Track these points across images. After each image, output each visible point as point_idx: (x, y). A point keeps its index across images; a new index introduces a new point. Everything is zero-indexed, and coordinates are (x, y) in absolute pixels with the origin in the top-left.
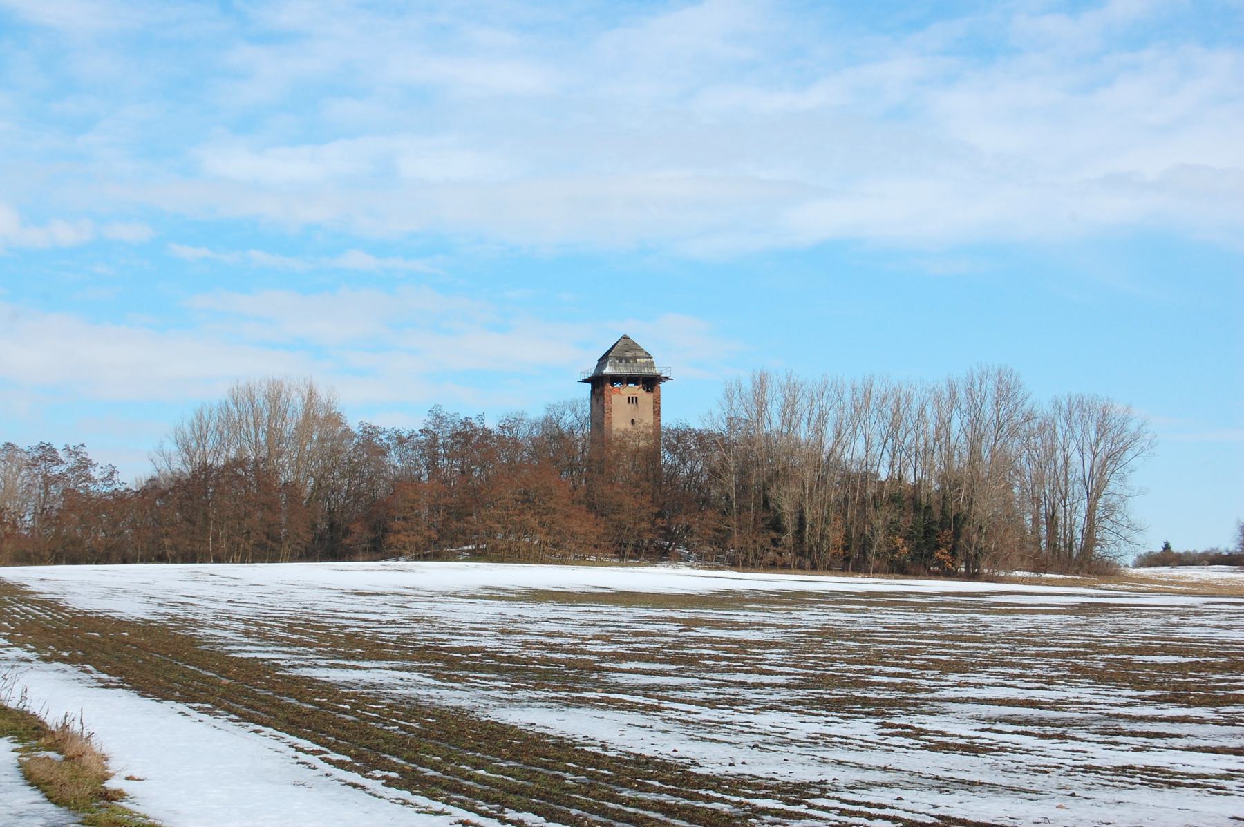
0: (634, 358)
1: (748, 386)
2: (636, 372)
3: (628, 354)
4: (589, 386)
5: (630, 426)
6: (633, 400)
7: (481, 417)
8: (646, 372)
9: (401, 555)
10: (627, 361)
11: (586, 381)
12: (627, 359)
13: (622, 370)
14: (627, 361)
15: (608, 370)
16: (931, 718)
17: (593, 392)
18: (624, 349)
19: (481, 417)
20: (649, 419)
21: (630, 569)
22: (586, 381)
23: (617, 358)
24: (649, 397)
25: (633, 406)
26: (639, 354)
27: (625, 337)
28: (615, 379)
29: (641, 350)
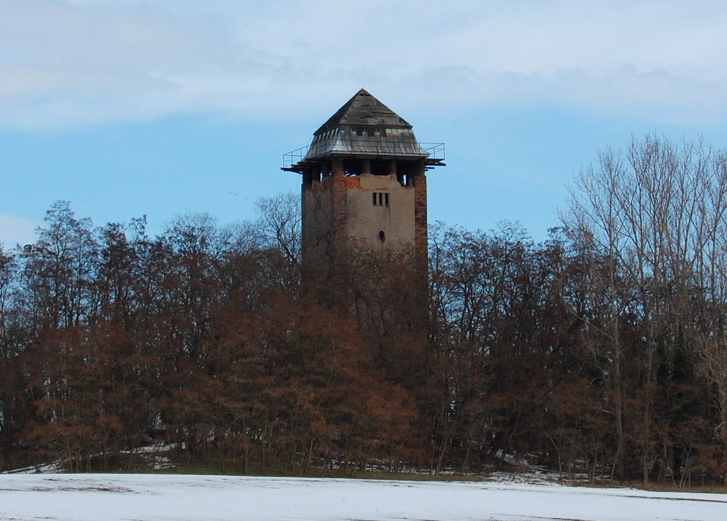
0: (382, 128)
1: (598, 168)
2: (387, 150)
3: (372, 122)
4: (298, 178)
5: (376, 242)
6: (381, 199)
7: (141, 222)
8: (403, 151)
9: (48, 460)
10: (371, 134)
11: (295, 169)
12: (371, 130)
13: (363, 148)
14: (371, 134)
15: (339, 147)
16: (39, 485)
17: (304, 187)
18: (362, 114)
19: (141, 222)
20: (405, 233)
21: (467, 484)
22: (295, 169)
23: (353, 127)
24: (410, 195)
25: (382, 209)
26: (389, 122)
27: (363, 94)
28: (354, 164)
29: (392, 115)
